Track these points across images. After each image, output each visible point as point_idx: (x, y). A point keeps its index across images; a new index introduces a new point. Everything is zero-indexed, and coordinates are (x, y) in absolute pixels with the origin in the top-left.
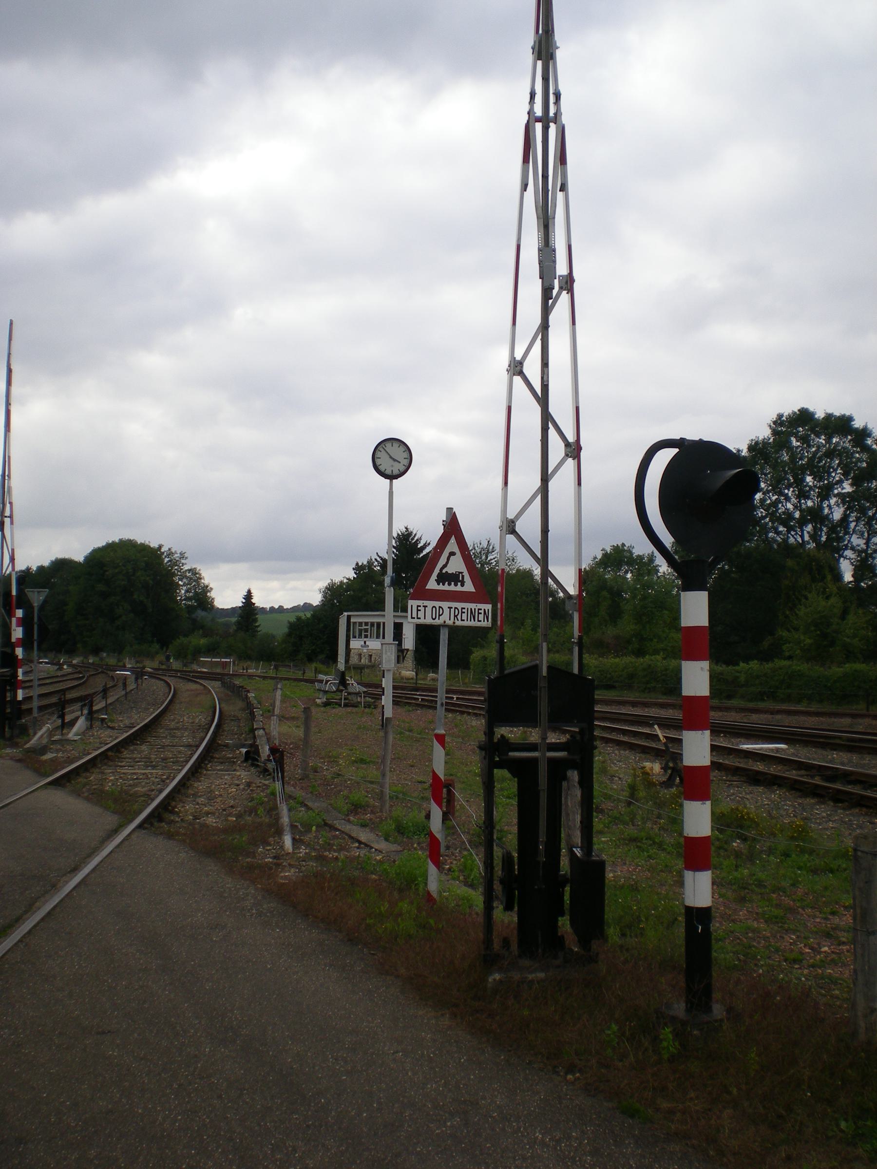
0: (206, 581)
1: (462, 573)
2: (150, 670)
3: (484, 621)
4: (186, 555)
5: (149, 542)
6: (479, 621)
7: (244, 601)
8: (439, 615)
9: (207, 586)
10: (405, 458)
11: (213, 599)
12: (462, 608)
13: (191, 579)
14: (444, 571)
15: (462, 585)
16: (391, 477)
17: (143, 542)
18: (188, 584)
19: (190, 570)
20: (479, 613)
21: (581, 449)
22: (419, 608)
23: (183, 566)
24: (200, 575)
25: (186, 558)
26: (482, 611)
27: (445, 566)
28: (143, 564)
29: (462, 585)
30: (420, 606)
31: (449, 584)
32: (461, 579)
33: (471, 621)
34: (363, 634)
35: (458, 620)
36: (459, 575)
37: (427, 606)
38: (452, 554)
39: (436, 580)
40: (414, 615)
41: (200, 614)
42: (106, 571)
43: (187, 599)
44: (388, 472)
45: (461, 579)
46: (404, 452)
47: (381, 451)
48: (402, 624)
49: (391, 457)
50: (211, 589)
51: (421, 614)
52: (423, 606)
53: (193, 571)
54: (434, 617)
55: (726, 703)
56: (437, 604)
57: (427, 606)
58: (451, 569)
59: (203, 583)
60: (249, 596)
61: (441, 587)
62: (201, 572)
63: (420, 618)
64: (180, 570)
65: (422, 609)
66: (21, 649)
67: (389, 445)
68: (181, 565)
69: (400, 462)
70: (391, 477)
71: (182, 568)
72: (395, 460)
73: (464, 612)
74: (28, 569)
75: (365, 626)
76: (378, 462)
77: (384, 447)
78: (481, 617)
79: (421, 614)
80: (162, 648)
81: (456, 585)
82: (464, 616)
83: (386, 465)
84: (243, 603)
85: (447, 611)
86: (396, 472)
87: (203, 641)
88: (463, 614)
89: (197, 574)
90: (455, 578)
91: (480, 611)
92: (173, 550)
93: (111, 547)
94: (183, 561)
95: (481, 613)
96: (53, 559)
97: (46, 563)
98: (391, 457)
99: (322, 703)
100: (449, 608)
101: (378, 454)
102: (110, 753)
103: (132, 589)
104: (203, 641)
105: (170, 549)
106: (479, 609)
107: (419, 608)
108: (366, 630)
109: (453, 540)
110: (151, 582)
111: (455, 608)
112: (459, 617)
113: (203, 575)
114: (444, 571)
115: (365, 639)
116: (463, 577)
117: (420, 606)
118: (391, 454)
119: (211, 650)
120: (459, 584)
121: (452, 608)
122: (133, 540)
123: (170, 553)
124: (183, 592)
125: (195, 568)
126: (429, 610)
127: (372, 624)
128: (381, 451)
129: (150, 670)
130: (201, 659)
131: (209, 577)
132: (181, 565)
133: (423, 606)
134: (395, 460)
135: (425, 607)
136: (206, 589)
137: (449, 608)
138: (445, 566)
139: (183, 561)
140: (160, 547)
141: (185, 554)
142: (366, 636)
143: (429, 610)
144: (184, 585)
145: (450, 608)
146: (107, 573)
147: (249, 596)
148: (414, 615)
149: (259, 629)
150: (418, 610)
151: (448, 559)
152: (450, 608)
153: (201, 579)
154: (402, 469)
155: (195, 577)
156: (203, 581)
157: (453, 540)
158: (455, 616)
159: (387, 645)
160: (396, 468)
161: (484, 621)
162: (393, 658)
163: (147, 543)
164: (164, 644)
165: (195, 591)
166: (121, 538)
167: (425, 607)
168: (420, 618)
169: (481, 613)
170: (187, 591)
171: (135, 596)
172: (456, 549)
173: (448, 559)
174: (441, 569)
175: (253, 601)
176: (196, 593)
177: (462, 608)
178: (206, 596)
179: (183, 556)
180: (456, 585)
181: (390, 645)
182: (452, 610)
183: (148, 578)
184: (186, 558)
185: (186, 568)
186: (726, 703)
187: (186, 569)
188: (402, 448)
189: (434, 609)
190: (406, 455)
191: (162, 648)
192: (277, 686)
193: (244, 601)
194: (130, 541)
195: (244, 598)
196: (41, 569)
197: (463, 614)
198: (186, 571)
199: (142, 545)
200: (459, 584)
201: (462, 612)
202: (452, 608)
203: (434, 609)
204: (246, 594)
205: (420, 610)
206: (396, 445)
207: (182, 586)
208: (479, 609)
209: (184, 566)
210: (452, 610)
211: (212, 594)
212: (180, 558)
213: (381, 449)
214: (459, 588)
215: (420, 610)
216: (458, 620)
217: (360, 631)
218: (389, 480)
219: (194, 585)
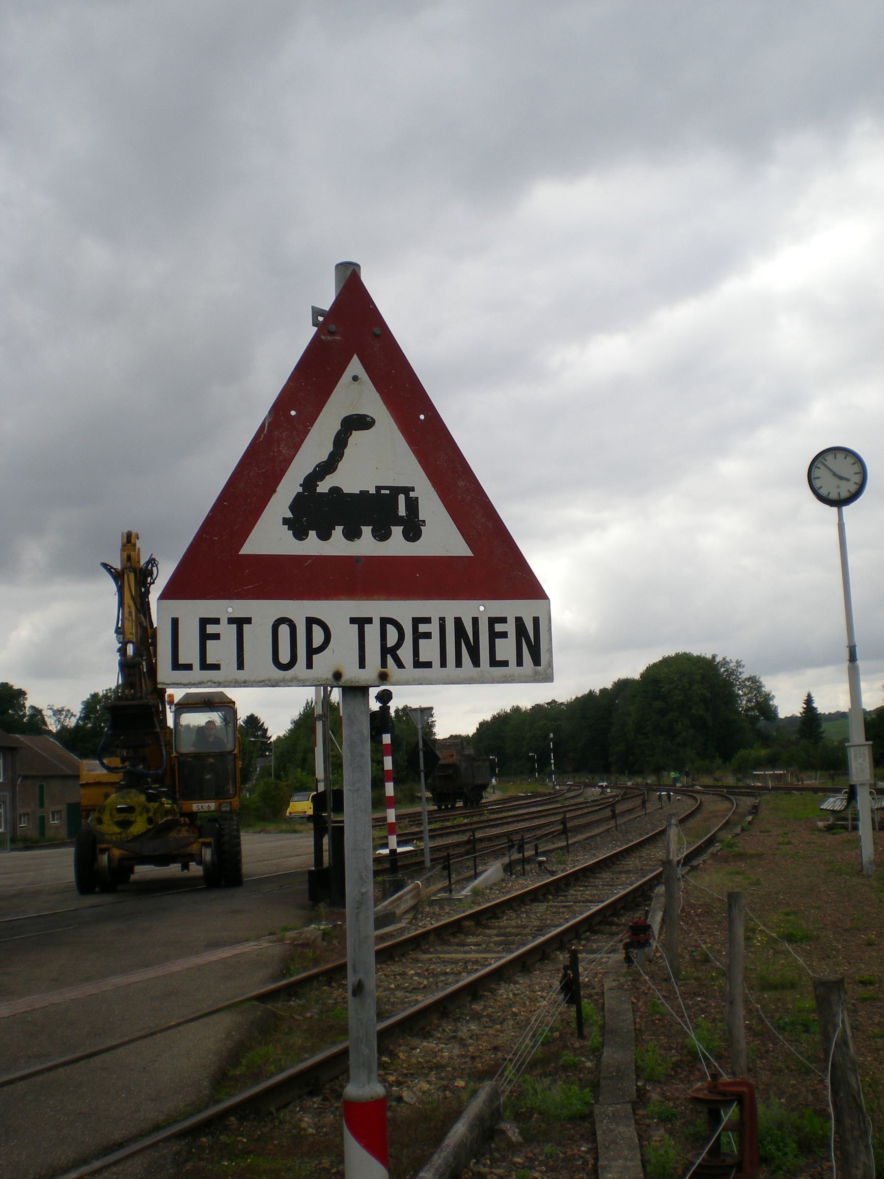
0: (766, 689)
1: (406, 490)
2: (699, 788)
3: (520, 663)
4: (743, 663)
5: (706, 654)
7: (805, 706)
8: (311, 652)
9: (769, 694)
10: (855, 473)
11: (776, 707)
12: (416, 621)
13: (751, 688)
14: (323, 487)
15: (413, 532)
16: (839, 503)
17: (699, 654)
18: (748, 694)
19: (748, 679)
20: (494, 636)
22: (211, 629)
23: (740, 674)
24: (760, 683)
25: (743, 666)
26: (510, 627)
28: (699, 677)
30: (216, 621)
31: (352, 534)
32: (402, 511)
33: (459, 664)
35: (400, 665)
37: (248, 621)
39: (286, 521)
40: (189, 652)
41: (762, 723)
42: (662, 687)
43: (748, 709)
44: (833, 496)
45: (402, 511)
46: (853, 464)
47: (819, 468)
49: (835, 475)
50: (774, 696)
52: (231, 621)
53: (753, 679)
54: (284, 658)
57: (248, 621)
59: (765, 692)
60: (809, 701)
62: (761, 680)
63: (216, 667)
64: (738, 678)
65: (228, 632)
66: (392, 783)
67: (829, 458)
68: (738, 674)
69: (848, 480)
70: (839, 503)
71: (740, 677)
72: (841, 478)
73: (428, 635)
74: (591, 693)
76: (817, 484)
77: (823, 461)
78: (506, 649)
80: (725, 762)
81: (382, 535)
82: (429, 650)
83: (831, 489)
84: (804, 708)
86: (844, 495)
87: (763, 752)
88: (422, 642)
89: (757, 682)
91: (499, 628)
92: (728, 659)
93: (666, 662)
94: (740, 670)
95: (504, 635)
96: (616, 680)
97: (609, 686)
98: (835, 475)
99: (825, 827)
100: (353, 621)
101: (816, 473)
102: (467, 923)
103: (690, 704)
104: (763, 752)
105: (724, 659)
106: (492, 621)
107: (211, 629)
110: (709, 695)
111: (385, 621)
112: (405, 653)
113: (763, 683)
114: (323, 487)
116: (413, 505)
117: (216, 621)
118: (834, 470)
119: (772, 762)
120: (397, 531)
121: (369, 621)
122: (690, 653)
123: (725, 662)
124: (744, 702)
125: (754, 676)
128: (819, 468)
129: (699, 788)
130: (755, 773)
131: (769, 684)
132: (738, 674)
133: (231, 621)
134: (841, 478)
135: (240, 623)
136: (768, 697)
137: (353, 621)
139: (740, 670)
140: (714, 657)
141: (742, 662)
144: (745, 694)
145: (361, 622)
146: (663, 689)
147: (809, 701)
148: (189, 652)
149: (824, 735)
150: (205, 637)
151: (340, 443)
152: (361, 622)
153: (762, 687)
154: (853, 488)
155: (755, 684)
156: (763, 689)
158: (386, 651)
159: (857, 748)
160: (845, 489)
161: (520, 663)
162: (868, 765)
163: (703, 655)
164: (726, 757)
165: (757, 701)
166: (678, 652)
167: (240, 623)
168: (216, 667)
169: (504, 635)
170: (749, 701)
171: (694, 711)
173: (340, 443)
174: (311, 481)
175: (815, 705)
176: (757, 702)
177: (416, 621)
178: (769, 704)
179: (739, 664)
181: (861, 748)
182: (372, 632)
183: (705, 691)
184: (743, 666)
185: (744, 676)
187: (745, 677)
188: (850, 460)
189: (284, 630)
190: (857, 468)
191: (725, 762)
192: (670, 822)
193: (805, 706)
194: (685, 654)
195: (804, 703)
196: (604, 691)
197: (422, 642)
198: (746, 679)
199: (698, 657)
200: (397, 531)
201: (418, 636)
202: (369, 621)
203: (284, 630)
204: (806, 698)
205: (216, 637)
206: (840, 456)
207: (742, 696)
208: (492, 621)
209: (742, 675)
210: (372, 632)
211: (775, 702)
212: (737, 667)
213: (820, 465)
215: (216, 637)
216: (400, 665)
218: (837, 508)
219: (755, 695)
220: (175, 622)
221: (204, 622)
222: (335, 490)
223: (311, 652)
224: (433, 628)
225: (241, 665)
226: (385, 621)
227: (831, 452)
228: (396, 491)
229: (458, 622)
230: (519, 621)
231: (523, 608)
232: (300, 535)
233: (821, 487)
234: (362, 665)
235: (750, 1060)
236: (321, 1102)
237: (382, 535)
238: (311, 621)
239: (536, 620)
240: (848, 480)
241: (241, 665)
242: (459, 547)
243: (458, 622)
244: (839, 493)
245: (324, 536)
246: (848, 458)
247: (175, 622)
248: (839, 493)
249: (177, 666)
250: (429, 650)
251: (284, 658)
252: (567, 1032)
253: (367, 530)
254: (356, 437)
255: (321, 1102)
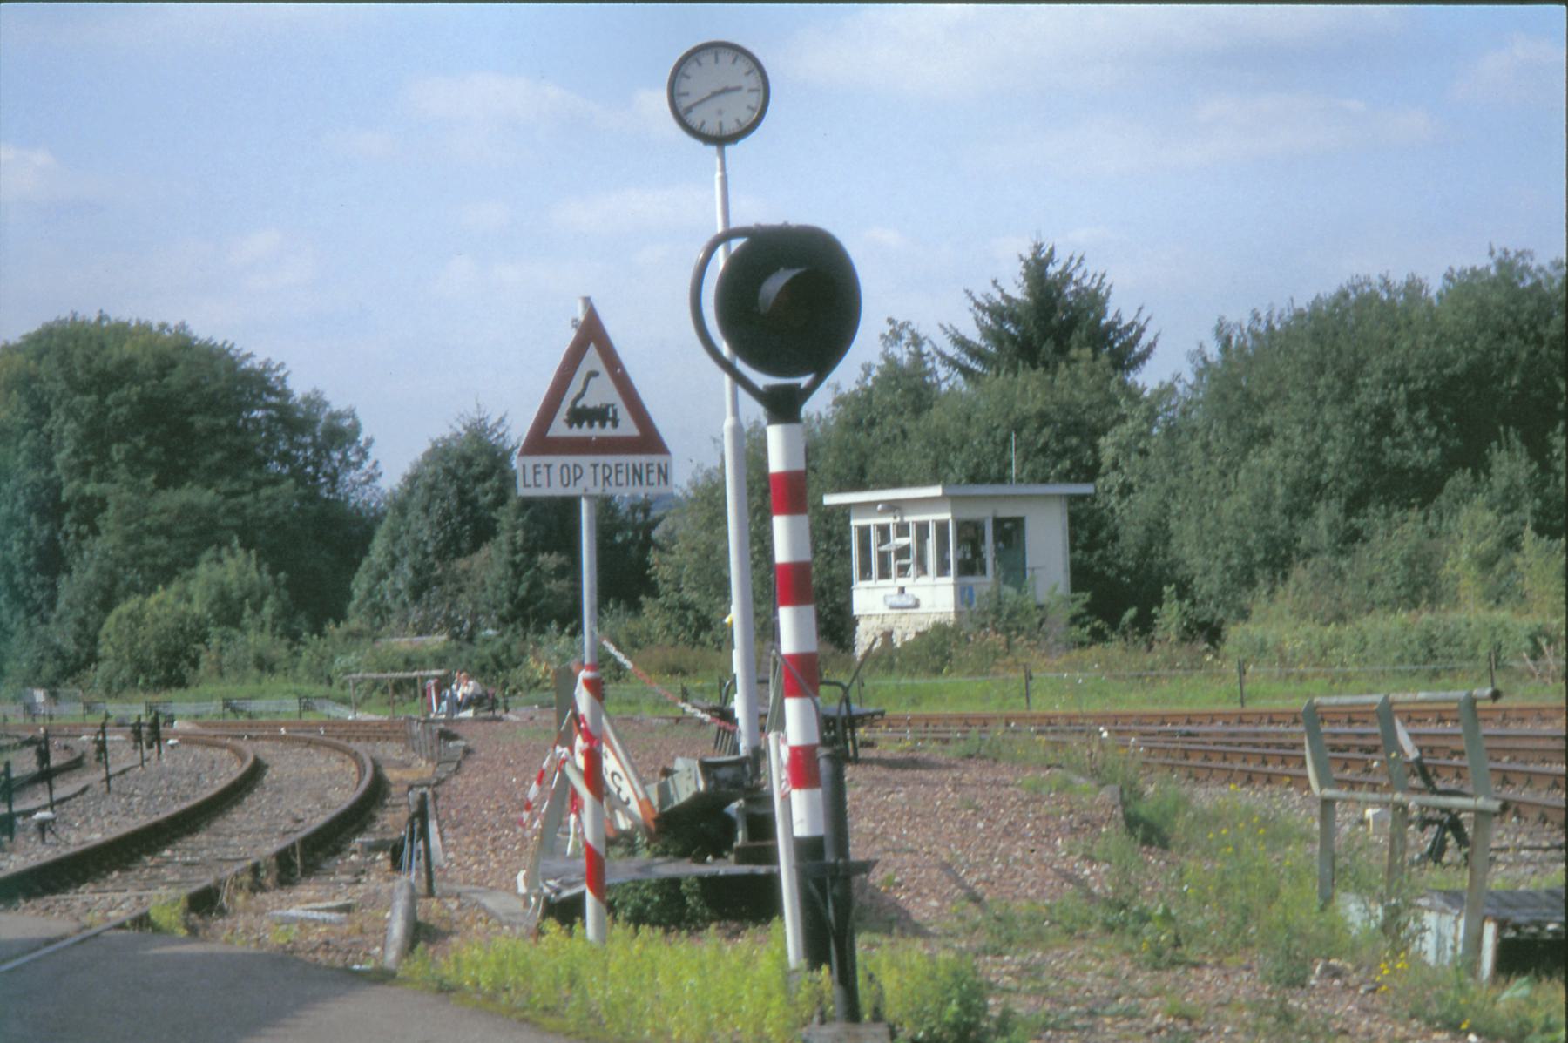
8: (576, 479)
15: (615, 423)
20: (649, 472)
26: (655, 468)
31: (591, 425)
32: (611, 415)
40: (530, 480)
65: (544, 470)
70: (720, 140)
78: (654, 477)
81: (603, 425)
82: (622, 478)
106: (648, 465)
114: (579, 405)
116: (615, 412)
135: (548, 466)
148: (530, 480)
150: (535, 473)
151: (586, 383)
152: (595, 466)
167: (548, 466)
173: (586, 383)
182: (599, 469)
200: (609, 424)
203: (565, 470)
210: (599, 469)
220: (524, 467)
221: (535, 466)
222: (584, 407)
223: (576, 479)
224: (624, 468)
225: (549, 485)
226: (604, 466)
228: (608, 406)
229: (634, 466)
231: (656, 459)
232: (571, 426)
233: (703, 124)
234: (595, 484)
235: (999, 732)
237: (603, 425)
238: (575, 466)
241: (549, 485)
243: (634, 466)
244: (721, 124)
245: (580, 425)
247: (524, 467)
248: (721, 124)
250: (622, 478)
251: (565, 482)
252: (95, 531)
254: (593, 381)
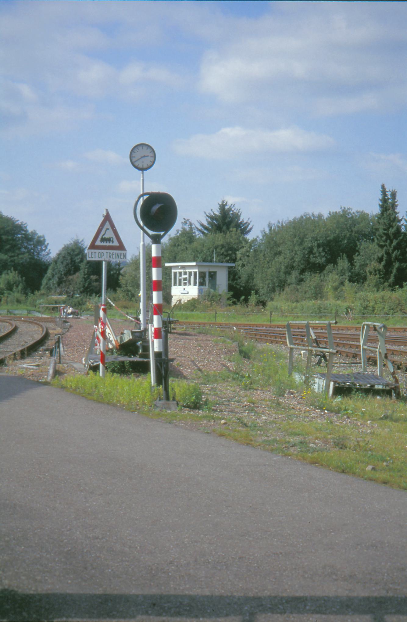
1: (112, 237)
6: (121, 258)
15: (113, 243)
21: (146, 170)
26: (123, 254)
27: (104, 234)
29: (113, 243)
31: (106, 243)
34: (182, 282)
36: (111, 238)
38: (108, 229)
40: (90, 256)
48: (215, 273)
51: (93, 256)
55: (362, 337)
56: (101, 251)
58: (107, 236)
61: (102, 244)
70: (143, 169)
75: (184, 275)
78: (122, 257)
79: (93, 256)
81: (109, 243)
82: (114, 256)
85: (105, 254)
90: (109, 240)
108: (185, 279)
109: (108, 223)
111: (110, 253)
112: (111, 257)
114: (104, 237)
115: (185, 287)
116: (113, 239)
120: (111, 242)
126: (97, 254)
127: (190, 273)
138: (104, 234)
142: (185, 284)
143: (97, 254)
145: (107, 253)
148: (90, 256)
150: (92, 254)
151: (106, 231)
152: (107, 253)
154: (152, 159)
157: (108, 223)
158: (110, 257)
167: (95, 252)
172: (109, 227)
173: (106, 231)
180: (109, 243)
182: (108, 254)
186: (362, 337)
200: (111, 242)
210: (108, 254)
214: (111, 244)
217: (180, 280)
222: (105, 238)
223: (102, 256)
227: (150, 166)
229: (117, 254)
230: (124, 254)
231: (123, 252)
232: (101, 242)
236: (397, 225)
239: (125, 254)
240: (148, 156)
242: (118, 245)
245: (104, 242)
246: (151, 153)
249: (89, 257)
250: (114, 256)
253: (108, 242)
254: (107, 231)
255: (397, 225)
